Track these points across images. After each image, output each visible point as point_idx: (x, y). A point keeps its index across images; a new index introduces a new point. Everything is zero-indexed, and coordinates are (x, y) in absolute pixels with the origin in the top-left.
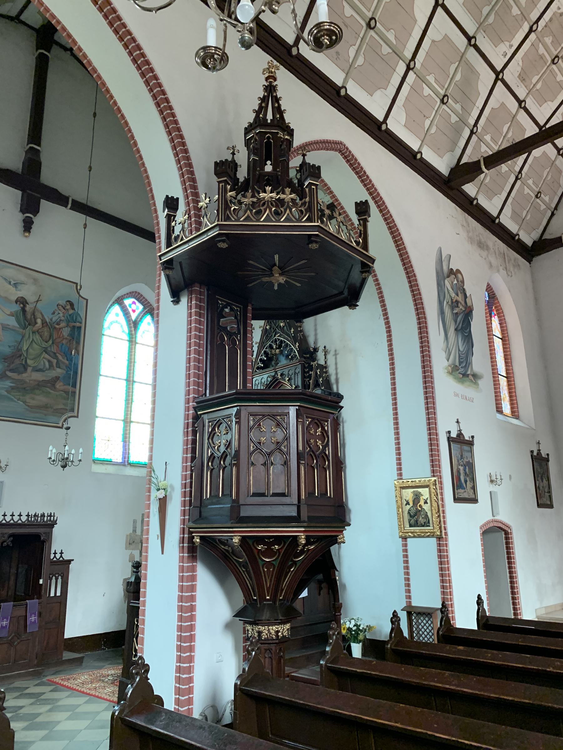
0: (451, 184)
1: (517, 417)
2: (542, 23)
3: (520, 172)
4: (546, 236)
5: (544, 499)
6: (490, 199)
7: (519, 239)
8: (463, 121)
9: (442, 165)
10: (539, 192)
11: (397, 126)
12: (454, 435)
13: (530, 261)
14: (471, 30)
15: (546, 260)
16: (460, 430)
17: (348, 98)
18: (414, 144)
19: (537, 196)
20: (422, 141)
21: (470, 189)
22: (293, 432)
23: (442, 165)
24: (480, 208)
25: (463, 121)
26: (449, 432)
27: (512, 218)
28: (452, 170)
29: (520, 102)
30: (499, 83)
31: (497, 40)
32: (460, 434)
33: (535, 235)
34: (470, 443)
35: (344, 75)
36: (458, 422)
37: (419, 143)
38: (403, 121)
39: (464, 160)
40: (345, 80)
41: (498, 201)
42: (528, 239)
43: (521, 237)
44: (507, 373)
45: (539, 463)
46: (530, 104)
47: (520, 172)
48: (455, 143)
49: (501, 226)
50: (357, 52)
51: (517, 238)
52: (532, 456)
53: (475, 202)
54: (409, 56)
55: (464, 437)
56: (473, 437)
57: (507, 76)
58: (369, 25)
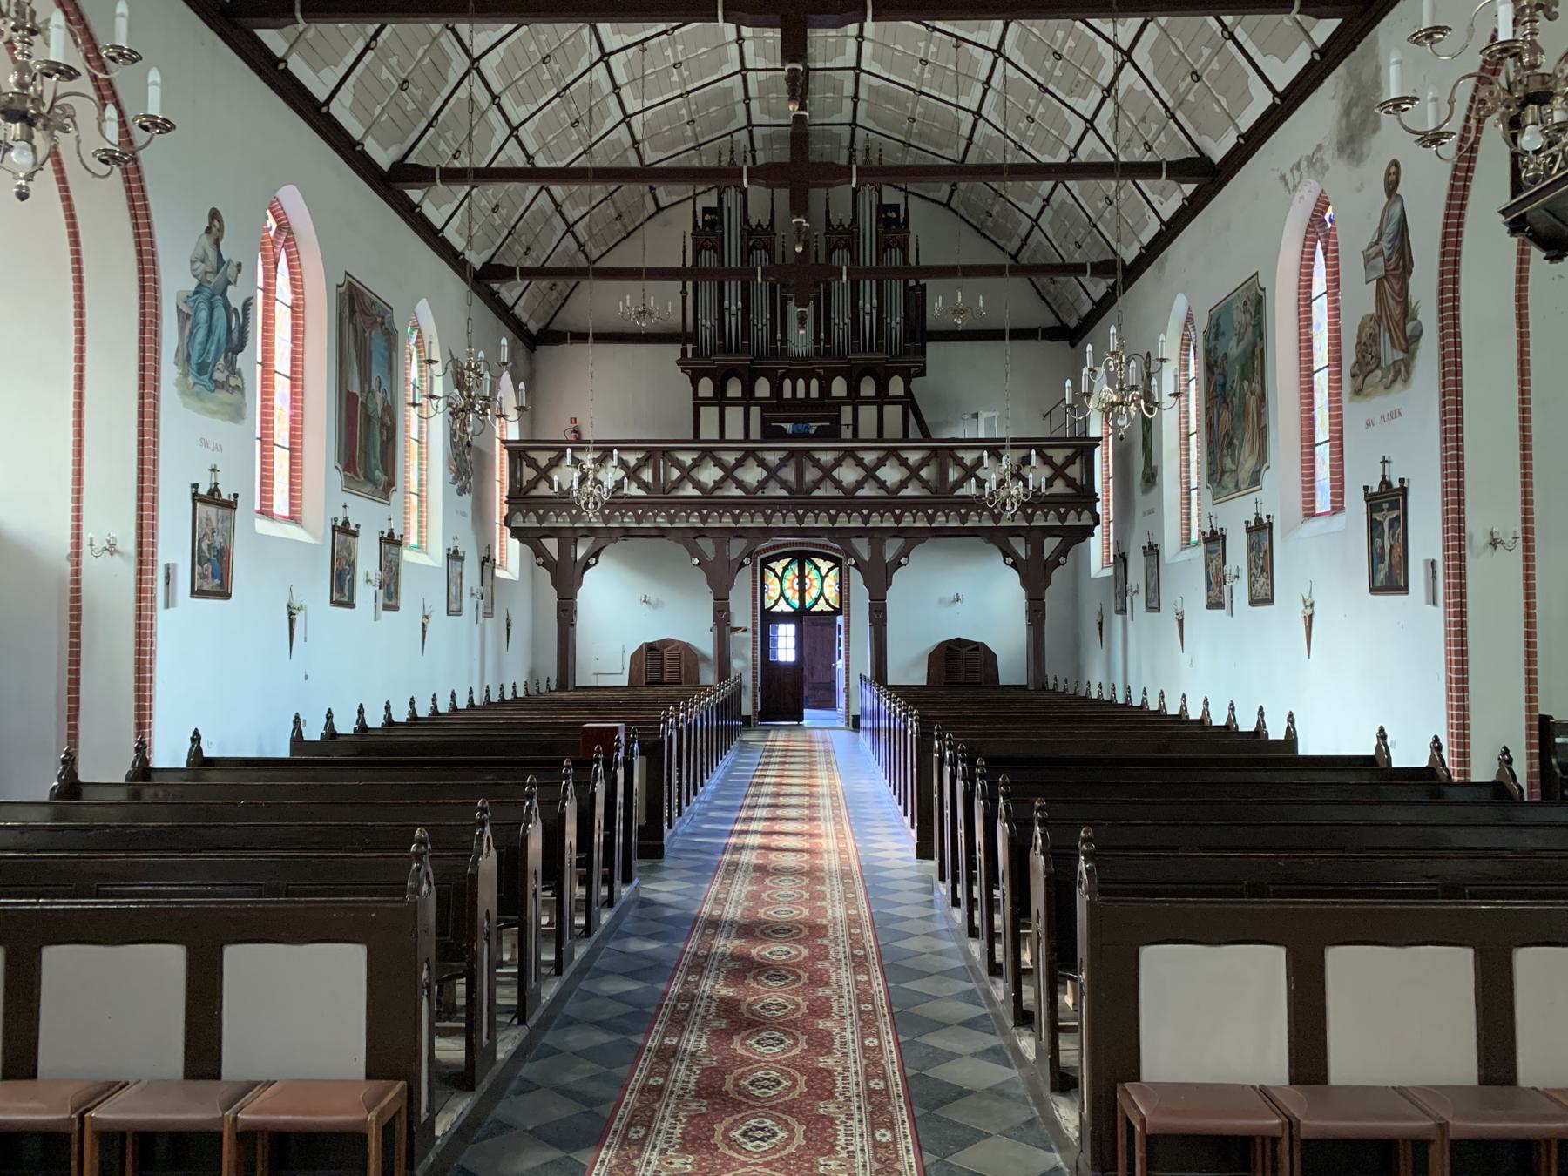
4: (553, 327)
7: (286, 70)
9: (476, 260)
10: (405, 81)
11: (340, 110)
12: (203, 491)
14: (497, 89)
17: (288, 74)
19: (494, 211)
21: (415, 195)
23: (384, 158)
24: (365, 156)
26: (196, 486)
27: (352, 110)
28: (394, 164)
29: (494, 97)
32: (214, 491)
33: (541, 325)
37: (286, 47)
38: (348, 104)
39: (411, 160)
40: (288, 53)
42: (533, 327)
43: (368, 149)
44: (292, 372)
46: (506, 101)
48: (406, 136)
49: (445, 242)
51: (281, 66)
56: (236, 496)
57: (523, 132)
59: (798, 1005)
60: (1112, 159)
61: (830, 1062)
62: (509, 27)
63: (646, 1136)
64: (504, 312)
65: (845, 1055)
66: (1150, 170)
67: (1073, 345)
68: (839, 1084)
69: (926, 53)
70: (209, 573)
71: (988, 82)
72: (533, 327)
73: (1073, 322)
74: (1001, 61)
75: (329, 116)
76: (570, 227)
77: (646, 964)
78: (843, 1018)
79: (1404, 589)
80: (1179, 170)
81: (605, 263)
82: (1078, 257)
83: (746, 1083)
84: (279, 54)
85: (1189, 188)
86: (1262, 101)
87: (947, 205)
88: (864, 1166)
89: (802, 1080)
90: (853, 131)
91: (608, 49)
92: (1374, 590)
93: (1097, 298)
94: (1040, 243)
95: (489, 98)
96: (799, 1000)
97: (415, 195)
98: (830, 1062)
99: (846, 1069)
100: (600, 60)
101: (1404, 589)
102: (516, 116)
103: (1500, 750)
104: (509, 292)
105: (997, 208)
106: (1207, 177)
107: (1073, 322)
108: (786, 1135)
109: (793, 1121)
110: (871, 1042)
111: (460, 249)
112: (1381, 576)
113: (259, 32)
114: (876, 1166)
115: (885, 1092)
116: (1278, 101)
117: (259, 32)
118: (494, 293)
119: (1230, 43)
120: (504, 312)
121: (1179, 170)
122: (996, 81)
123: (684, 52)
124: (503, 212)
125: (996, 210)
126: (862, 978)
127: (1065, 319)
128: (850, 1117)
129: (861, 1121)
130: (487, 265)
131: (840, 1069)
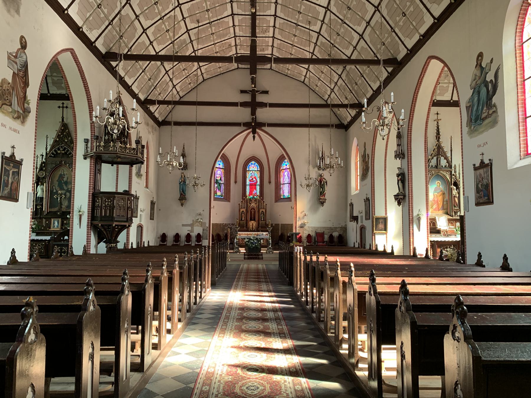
0: (145, 104)
1: (147, 188)
2: (165, 18)
3: (145, 69)
4: (167, 120)
5: (152, 218)
6: (91, 30)
8: (153, 85)
9: (142, 97)
13: (159, 127)
15: (166, 129)
16: (13, 153)
18: (80, 23)
20: (84, 22)
21: (114, 64)
22: (501, 289)
23: (142, 97)
25: (153, 85)
26: (4, 153)
30: (144, 34)
31: (147, 18)
32: (13, 155)
33: (163, 118)
34: (138, 199)
35: (83, 23)
36: (13, 147)
40: (125, 76)
41: (133, 80)
42: (160, 119)
45: (153, 203)
47: (145, 69)
48: (148, 91)
50: (91, 15)
52: (2, 156)
53: (81, 30)
54: (111, 19)
55: (15, 158)
58: (98, 6)
60: (358, 67)
62: (177, 63)
63: (202, 387)
64: (151, 115)
66: (376, 62)
67: (346, 131)
69: (300, 9)
71: (323, 21)
72: (160, 119)
73: (346, 123)
74: (328, 12)
75: (95, 47)
76: (174, 86)
79: (16, 200)
80: (353, 106)
81: (185, 99)
82: (346, 102)
84: (80, 26)
85: (390, 69)
86: (429, 21)
87: (303, 82)
90: (273, 40)
91: (189, 28)
93: (410, 47)
94: (334, 97)
95: (149, 43)
97: (114, 64)
100: (178, 6)
101: (16, 200)
102: (146, 24)
104: (152, 108)
105: (319, 83)
106: (397, 65)
107: (346, 123)
111: (80, 25)
113: (111, 62)
116: (409, 52)
117: (111, 62)
118: (148, 108)
119: (393, 33)
120: (151, 115)
121: (353, 106)
122: (308, 76)
123: (215, 30)
124: (162, 95)
125: (319, 84)
127: (343, 122)
130: (146, 99)
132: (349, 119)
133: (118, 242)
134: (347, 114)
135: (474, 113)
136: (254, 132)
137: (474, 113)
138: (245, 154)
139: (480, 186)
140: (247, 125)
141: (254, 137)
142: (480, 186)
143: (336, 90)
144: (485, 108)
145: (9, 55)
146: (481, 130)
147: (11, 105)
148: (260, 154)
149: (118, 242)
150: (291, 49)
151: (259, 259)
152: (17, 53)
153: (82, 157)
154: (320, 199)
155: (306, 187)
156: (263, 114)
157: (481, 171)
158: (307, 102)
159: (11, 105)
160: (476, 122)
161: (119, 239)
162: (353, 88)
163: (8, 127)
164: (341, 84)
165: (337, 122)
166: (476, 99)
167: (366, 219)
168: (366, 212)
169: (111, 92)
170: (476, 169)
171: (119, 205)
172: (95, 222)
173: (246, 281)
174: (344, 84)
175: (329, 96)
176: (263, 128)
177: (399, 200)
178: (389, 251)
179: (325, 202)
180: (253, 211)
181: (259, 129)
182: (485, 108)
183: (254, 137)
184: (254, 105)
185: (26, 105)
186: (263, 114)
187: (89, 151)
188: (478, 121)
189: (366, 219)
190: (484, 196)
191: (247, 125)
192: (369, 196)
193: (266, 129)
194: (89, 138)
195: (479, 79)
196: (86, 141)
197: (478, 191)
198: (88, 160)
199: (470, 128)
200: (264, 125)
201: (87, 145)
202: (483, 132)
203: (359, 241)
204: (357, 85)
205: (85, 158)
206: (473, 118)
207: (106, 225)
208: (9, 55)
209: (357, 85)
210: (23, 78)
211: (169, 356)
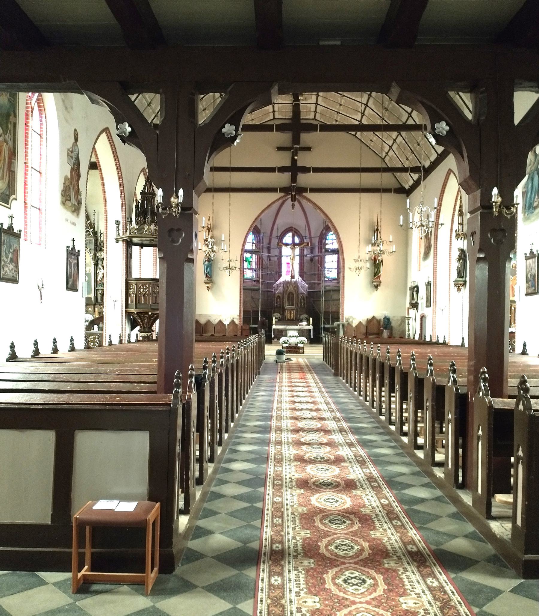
52: (67, 250)
59: (321, 520)
61: (303, 533)
65: (293, 514)
68: (302, 581)
70: (531, 286)
73: (407, 187)
77: (431, 517)
78: (293, 514)
79: (77, 290)
83: (347, 522)
88: (291, 602)
89: (329, 585)
92: (68, 289)
96: (321, 527)
98: (303, 533)
99: (294, 529)
101: (77, 290)
103: (53, 338)
108: (330, 548)
109: (328, 554)
110: (278, 521)
112: (70, 283)
114: (283, 602)
115: (273, 516)
126: (278, 499)
127: (404, 185)
128: (292, 506)
129: (287, 504)
131: (297, 529)
132: (411, 182)
133: (153, 331)
134: (408, 180)
135: (528, 200)
136: (293, 199)
137: (528, 200)
138: (282, 222)
139: (529, 276)
140: (285, 190)
141: (293, 206)
142: (529, 276)
143: (395, 147)
144: (537, 197)
145: (68, 150)
146: (533, 218)
147: (70, 200)
148: (300, 223)
149: (153, 331)
150: (339, 99)
151: (299, 352)
152: (72, 148)
153: (115, 241)
154: (373, 282)
155: (355, 270)
156: (304, 179)
157: (531, 261)
158: (357, 165)
159: (70, 200)
160: (529, 209)
161: (153, 328)
162: (415, 149)
163: (69, 221)
164: (401, 142)
165: (398, 186)
166: (530, 185)
167: (427, 306)
168: (427, 298)
169: (204, 218)
170: (527, 258)
171: (154, 292)
172: (130, 311)
173: (290, 372)
174: (404, 142)
175: (387, 153)
176: (304, 194)
177: (459, 287)
178: (441, 341)
179: (380, 285)
180: (291, 296)
181: (300, 196)
182: (537, 197)
183: (293, 206)
184: (294, 169)
185: (79, 196)
186: (304, 179)
187: (121, 235)
188: (531, 209)
189: (427, 306)
190: (532, 287)
191: (285, 190)
192: (431, 280)
193: (309, 195)
194: (121, 220)
195: (534, 165)
196: (118, 223)
197: (528, 281)
198: (120, 242)
199: (524, 215)
200: (305, 190)
201: (118, 227)
202: (534, 220)
203: (418, 332)
204: (419, 145)
205: (117, 242)
206: (527, 205)
207: (141, 313)
208: (68, 150)
209: (419, 145)
210: (76, 170)
211: (459, 191)
